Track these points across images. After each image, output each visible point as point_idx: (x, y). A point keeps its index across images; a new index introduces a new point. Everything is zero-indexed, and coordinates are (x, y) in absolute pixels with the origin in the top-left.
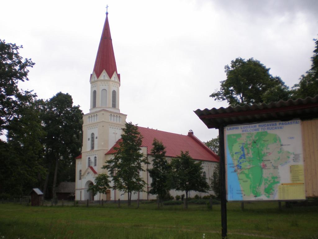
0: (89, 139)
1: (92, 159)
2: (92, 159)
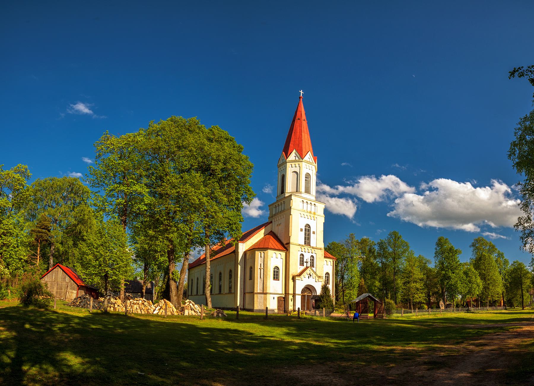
0: (301, 230)
1: (307, 257)
2: (307, 257)
